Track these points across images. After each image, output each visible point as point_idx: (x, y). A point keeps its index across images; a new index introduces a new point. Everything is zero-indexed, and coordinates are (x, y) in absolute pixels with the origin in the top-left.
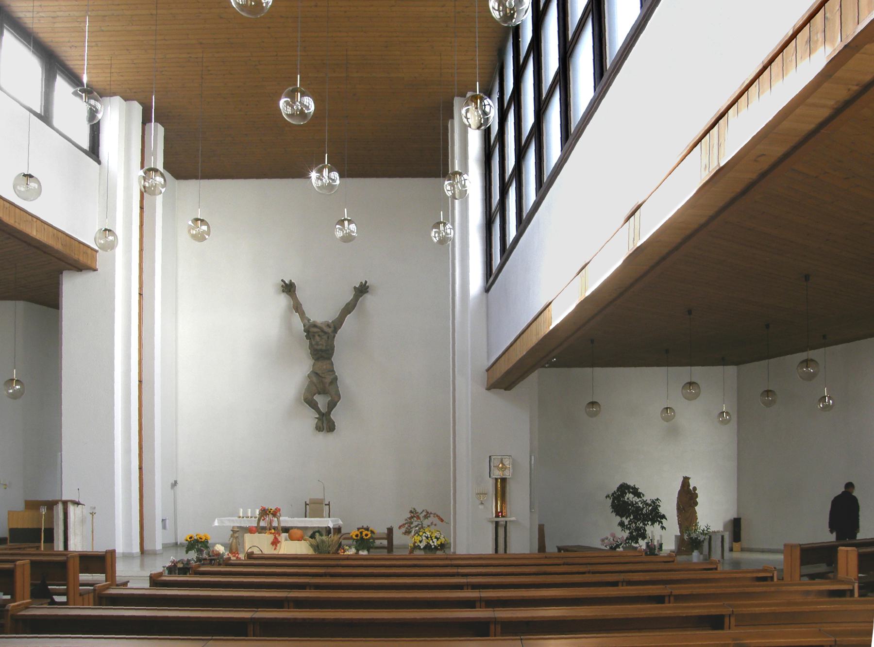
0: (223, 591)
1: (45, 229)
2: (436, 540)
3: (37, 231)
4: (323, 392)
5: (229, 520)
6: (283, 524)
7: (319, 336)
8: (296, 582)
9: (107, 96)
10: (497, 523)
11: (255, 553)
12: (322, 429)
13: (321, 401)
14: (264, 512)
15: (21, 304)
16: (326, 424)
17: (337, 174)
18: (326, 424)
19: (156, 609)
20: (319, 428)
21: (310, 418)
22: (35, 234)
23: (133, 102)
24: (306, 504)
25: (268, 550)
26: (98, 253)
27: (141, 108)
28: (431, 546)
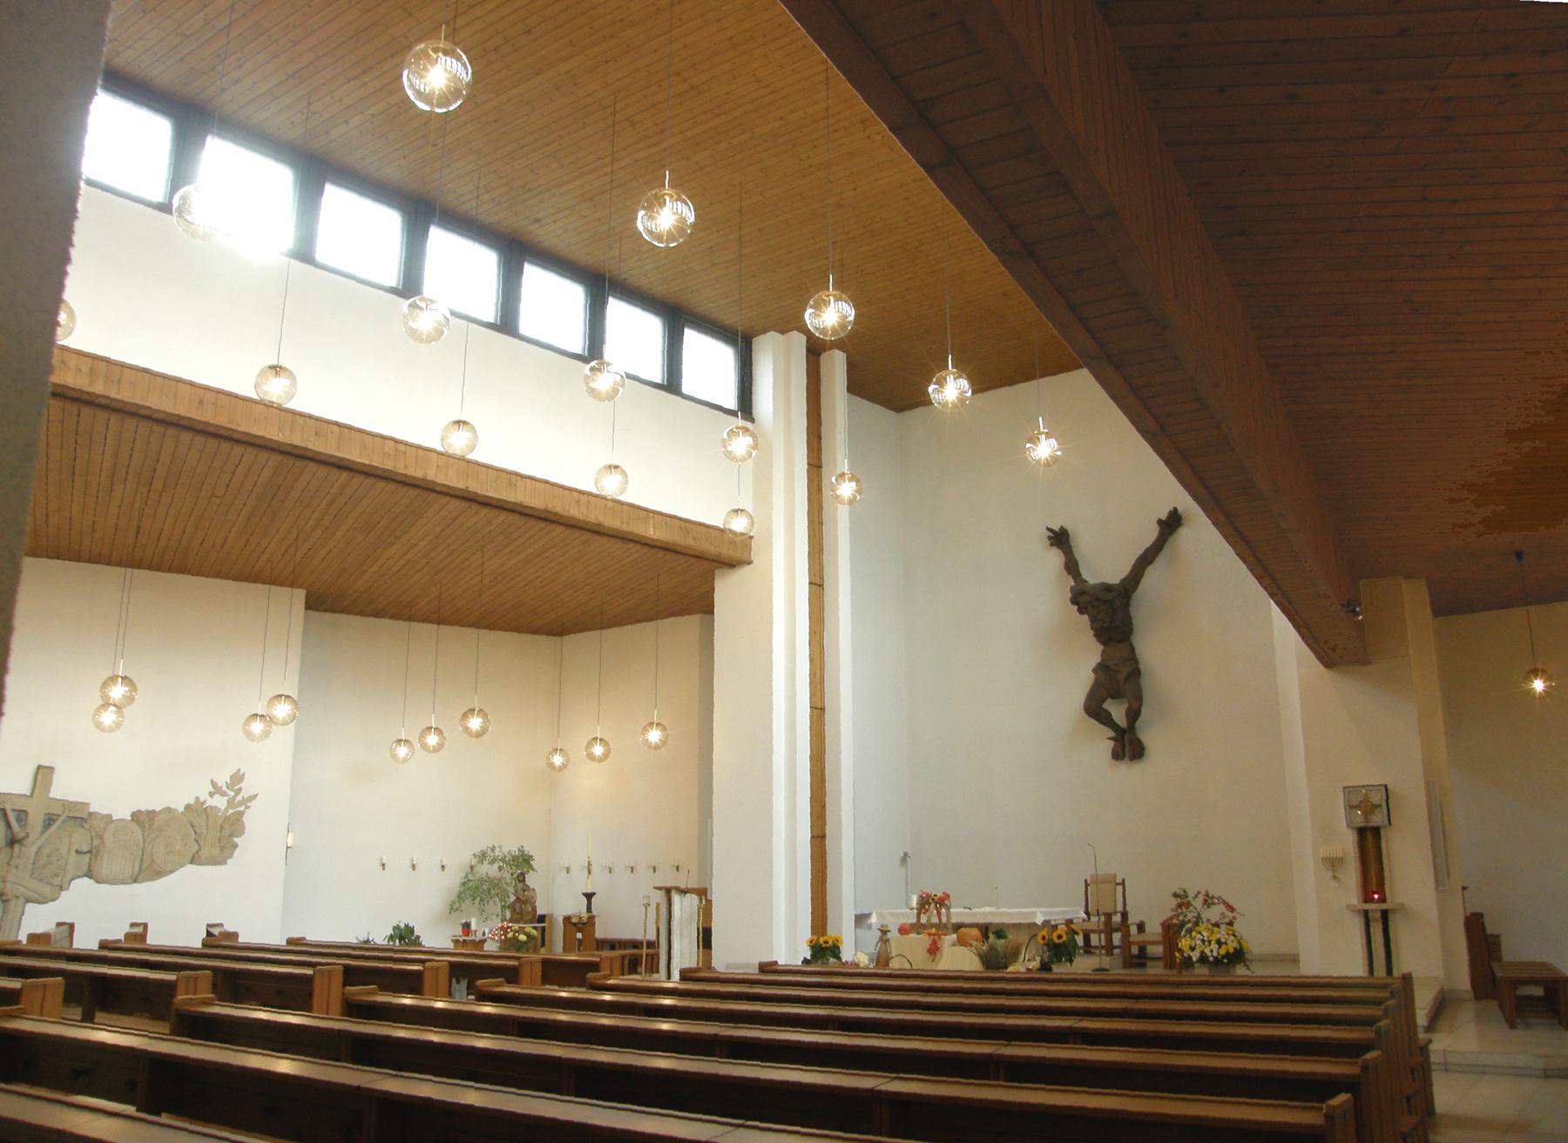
0: (884, 1038)
1: (666, 523)
2: (1217, 946)
3: (654, 528)
4: (1116, 695)
5: (892, 914)
6: (954, 920)
7: (1093, 607)
8: (900, 1020)
9: (758, 335)
10: (1366, 913)
11: (779, 963)
12: (1121, 755)
13: (1118, 711)
14: (925, 902)
15: (698, 616)
16: (1128, 746)
17: (966, 382)
18: (1128, 746)
19: (1271, 1105)
20: (1117, 755)
21: (1101, 742)
22: (652, 532)
23: (791, 333)
24: (1087, 885)
25: (921, 962)
26: (753, 541)
27: (805, 338)
28: (1207, 957)
